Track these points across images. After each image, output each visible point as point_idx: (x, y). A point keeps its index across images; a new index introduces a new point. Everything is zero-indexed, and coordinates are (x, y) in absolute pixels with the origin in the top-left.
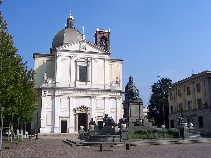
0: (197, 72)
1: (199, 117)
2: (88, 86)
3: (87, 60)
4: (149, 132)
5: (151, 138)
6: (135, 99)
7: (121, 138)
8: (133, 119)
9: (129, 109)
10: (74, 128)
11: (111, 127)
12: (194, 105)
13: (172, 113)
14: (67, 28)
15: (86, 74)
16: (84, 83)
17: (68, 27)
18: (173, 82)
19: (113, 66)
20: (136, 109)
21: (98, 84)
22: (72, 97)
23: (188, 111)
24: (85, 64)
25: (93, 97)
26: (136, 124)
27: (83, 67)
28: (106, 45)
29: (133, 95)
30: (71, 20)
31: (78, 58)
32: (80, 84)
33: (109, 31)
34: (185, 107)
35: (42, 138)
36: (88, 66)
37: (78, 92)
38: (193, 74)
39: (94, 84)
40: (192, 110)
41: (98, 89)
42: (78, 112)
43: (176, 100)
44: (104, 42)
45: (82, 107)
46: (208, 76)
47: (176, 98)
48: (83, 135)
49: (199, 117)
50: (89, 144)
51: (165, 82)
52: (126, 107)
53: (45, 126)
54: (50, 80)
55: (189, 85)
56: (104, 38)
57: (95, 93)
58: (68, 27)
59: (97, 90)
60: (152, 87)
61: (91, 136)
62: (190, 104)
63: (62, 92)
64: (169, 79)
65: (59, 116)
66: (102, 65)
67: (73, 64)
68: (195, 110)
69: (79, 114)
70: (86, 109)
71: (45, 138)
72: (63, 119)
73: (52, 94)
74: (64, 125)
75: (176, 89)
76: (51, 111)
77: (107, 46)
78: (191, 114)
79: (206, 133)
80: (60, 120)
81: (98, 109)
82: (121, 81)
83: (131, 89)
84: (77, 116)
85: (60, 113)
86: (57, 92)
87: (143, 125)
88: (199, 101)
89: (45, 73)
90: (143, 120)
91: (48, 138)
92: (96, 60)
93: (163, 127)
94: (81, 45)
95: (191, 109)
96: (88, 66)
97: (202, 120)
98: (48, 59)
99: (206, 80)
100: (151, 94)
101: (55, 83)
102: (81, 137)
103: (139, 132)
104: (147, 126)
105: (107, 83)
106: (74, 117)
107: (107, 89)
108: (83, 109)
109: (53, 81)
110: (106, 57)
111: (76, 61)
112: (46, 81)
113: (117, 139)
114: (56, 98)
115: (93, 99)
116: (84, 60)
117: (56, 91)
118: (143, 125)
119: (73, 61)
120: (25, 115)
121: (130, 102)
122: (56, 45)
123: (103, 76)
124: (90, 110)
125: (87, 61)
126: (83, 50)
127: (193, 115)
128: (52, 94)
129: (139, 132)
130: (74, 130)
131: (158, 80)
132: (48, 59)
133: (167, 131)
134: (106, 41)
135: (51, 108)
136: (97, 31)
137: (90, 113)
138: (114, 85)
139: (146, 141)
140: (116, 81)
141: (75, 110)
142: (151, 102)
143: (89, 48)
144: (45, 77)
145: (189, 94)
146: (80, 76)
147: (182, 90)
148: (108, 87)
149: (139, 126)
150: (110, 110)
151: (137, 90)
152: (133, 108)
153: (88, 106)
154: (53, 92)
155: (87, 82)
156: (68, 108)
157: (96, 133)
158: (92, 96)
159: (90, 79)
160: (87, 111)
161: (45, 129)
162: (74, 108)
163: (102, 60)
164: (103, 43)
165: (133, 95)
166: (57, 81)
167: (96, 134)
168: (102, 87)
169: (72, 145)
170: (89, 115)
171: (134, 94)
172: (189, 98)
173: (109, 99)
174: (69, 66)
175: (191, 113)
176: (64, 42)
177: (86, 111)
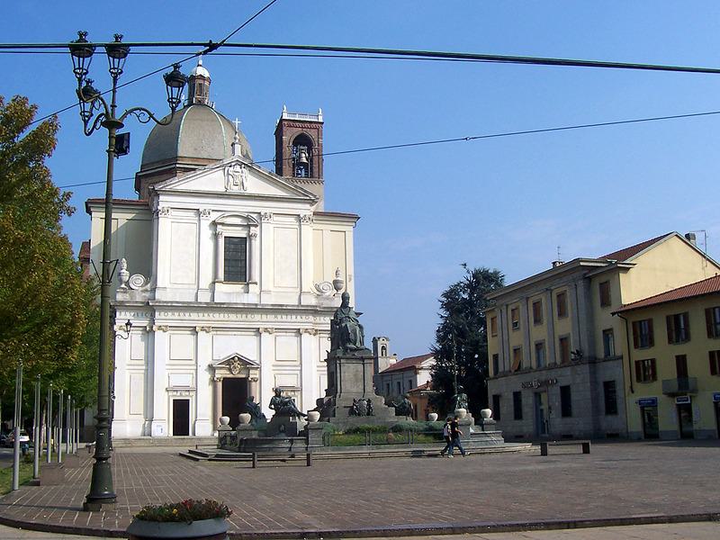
0: (567, 258)
1: (561, 387)
2: (251, 299)
3: (247, 218)
4: (384, 430)
5: (378, 444)
6: (352, 350)
7: (307, 443)
8: (346, 399)
9: (338, 375)
10: (210, 420)
11: (286, 418)
12: (552, 355)
13: (566, 364)
14: (188, 106)
15: (243, 262)
16: (238, 288)
17: (191, 103)
18: (508, 282)
19: (327, 234)
20: (355, 375)
21: (280, 290)
22: (203, 329)
23: (536, 371)
24: (242, 233)
25: (266, 330)
26: (353, 411)
27: (236, 240)
28: (312, 161)
29: (349, 341)
30: (201, 82)
31: (220, 214)
32: (228, 292)
33: (321, 120)
34: (529, 360)
35: (118, 450)
36: (250, 236)
37: (222, 315)
38: (554, 263)
39: (269, 292)
40: (545, 368)
41: (281, 305)
42: (222, 374)
43: (505, 338)
44: (304, 155)
45: (233, 358)
46: (585, 274)
47: (505, 332)
48: (228, 438)
49: (561, 387)
50: (236, 456)
51: (484, 281)
52: (333, 367)
53: (126, 416)
54: (138, 281)
55: (564, 289)
56: (303, 141)
57: (271, 317)
58: (191, 103)
59: (278, 310)
60: (446, 295)
61: (242, 440)
62: (541, 351)
63: (173, 317)
64: (496, 273)
65: (167, 386)
66: (293, 234)
67: (207, 233)
68: (553, 366)
69: (226, 381)
70: (246, 364)
71: (127, 450)
72: (179, 394)
73: (145, 323)
74: (181, 411)
75: (507, 306)
76: (143, 371)
77: (312, 164)
78: (543, 378)
79: (577, 433)
80: (169, 399)
81: (280, 364)
82: (350, 280)
83: (343, 325)
84: (220, 385)
85: (169, 379)
86: (159, 317)
87: (368, 414)
88: (564, 341)
89: (124, 260)
90: (369, 401)
91: (135, 450)
92: (276, 218)
93: (432, 418)
94: (228, 174)
95: (543, 365)
96: (250, 236)
97: (615, 392)
98: (130, 216)
99: (581, 283)
100: (442, 317)
101: (154, 290)
102: (222, 442)
103: (356, 431)
104: (377, 416)
105: (308, 286)
106: (210, 388)
107: (307, 306)
108: (236, 364)
109: (147, 284)
110: (305, 210)
111: (214, 224)
112: (127, 283)
113: (300, 445)
114: (158, 334)
115: (265, 335)
116: (238, 221)
117: (118, 313)
118: (368, 414)
119: (205, 223)
120: (82, 391)
121: (339, 358)
122: (153, 163)
123: (295, 266)
124: (259, 368)
125: (249, 222)
126: (235, 190)
127: (546, 383)
128: (145, 323)
129: (356, 431)
130: (211, 426)
131: (461, 276)
132: (130, 216)
133: (425, 426)
134: (310, 150)
135: (143, 362)
136: (281, 120)
137: (258, 376)
138: (327, 294)
139: (365, 450)
140: (335, 282)
141: (212, 368)
142: (440, 339)
143: (254, 185)
144: (124, 271)
145: (538, 321)
146: (227, 268)
147: (522, 309)
148: (310, 301)
149: (359, 415)
150: (315, 368)
151: (361, 327)
152: (349, 371)
153: (251, 355)
154: (149, 315)
155: (248, 284)
156: (194, 362)
157: (253, 432)
158: (262, 326)
159: (256, 277)
160: (249, 369)
161: (125, 425)
162: (209, 361)
163: (292, 219)
164: (300, 157)
165: (349, 341)
166: (159, 284)
167: (255, 435)
168: (292, 301)
169: (198, 460)
170: (253, 383)
171: (352, 336)
172: (539, 333)
173: (315, 335)
174: (193, 240)
175: (544, 375)
176: (180, 153)
177: (246, 372)
